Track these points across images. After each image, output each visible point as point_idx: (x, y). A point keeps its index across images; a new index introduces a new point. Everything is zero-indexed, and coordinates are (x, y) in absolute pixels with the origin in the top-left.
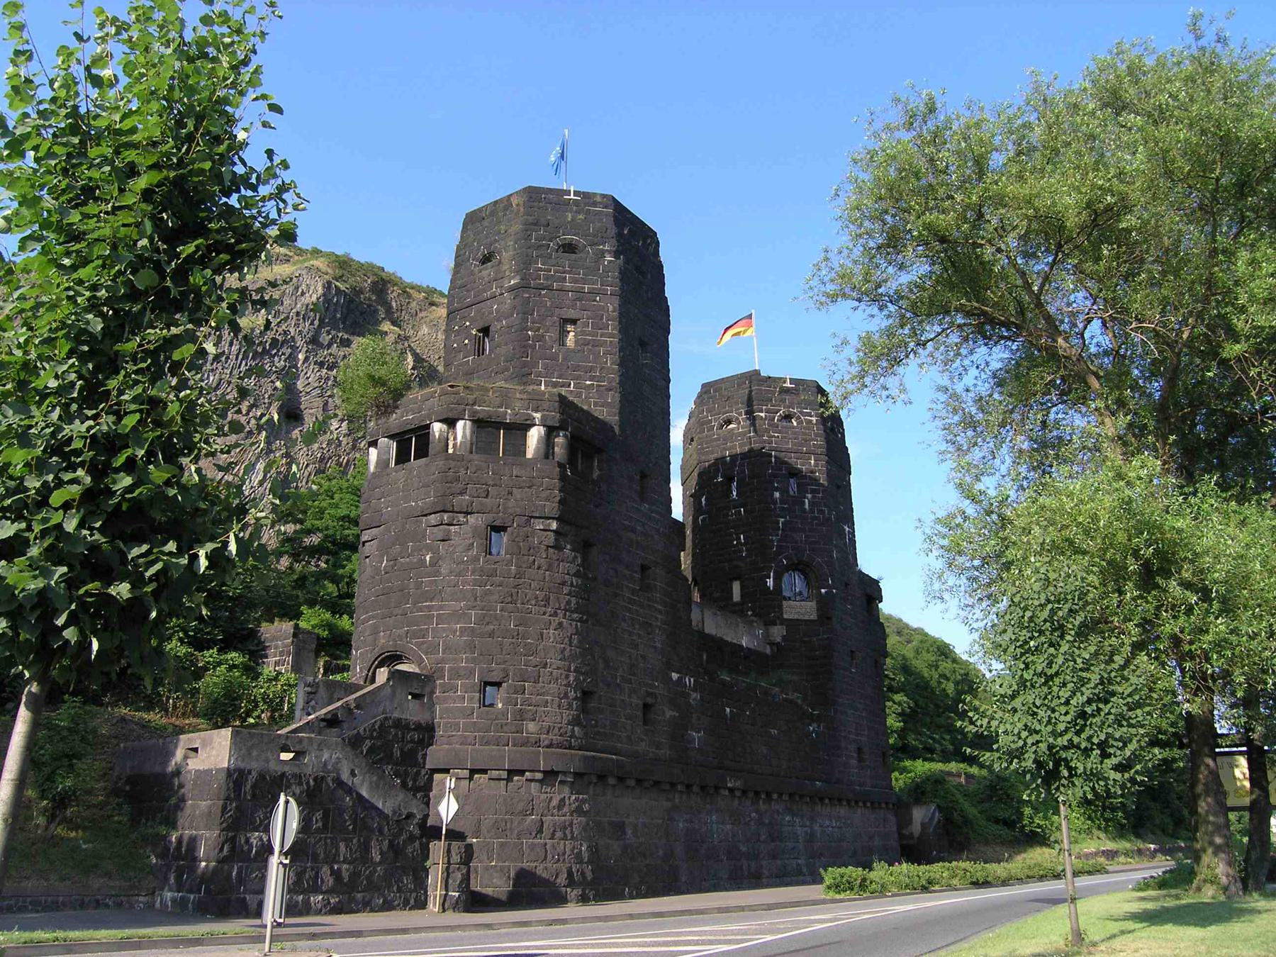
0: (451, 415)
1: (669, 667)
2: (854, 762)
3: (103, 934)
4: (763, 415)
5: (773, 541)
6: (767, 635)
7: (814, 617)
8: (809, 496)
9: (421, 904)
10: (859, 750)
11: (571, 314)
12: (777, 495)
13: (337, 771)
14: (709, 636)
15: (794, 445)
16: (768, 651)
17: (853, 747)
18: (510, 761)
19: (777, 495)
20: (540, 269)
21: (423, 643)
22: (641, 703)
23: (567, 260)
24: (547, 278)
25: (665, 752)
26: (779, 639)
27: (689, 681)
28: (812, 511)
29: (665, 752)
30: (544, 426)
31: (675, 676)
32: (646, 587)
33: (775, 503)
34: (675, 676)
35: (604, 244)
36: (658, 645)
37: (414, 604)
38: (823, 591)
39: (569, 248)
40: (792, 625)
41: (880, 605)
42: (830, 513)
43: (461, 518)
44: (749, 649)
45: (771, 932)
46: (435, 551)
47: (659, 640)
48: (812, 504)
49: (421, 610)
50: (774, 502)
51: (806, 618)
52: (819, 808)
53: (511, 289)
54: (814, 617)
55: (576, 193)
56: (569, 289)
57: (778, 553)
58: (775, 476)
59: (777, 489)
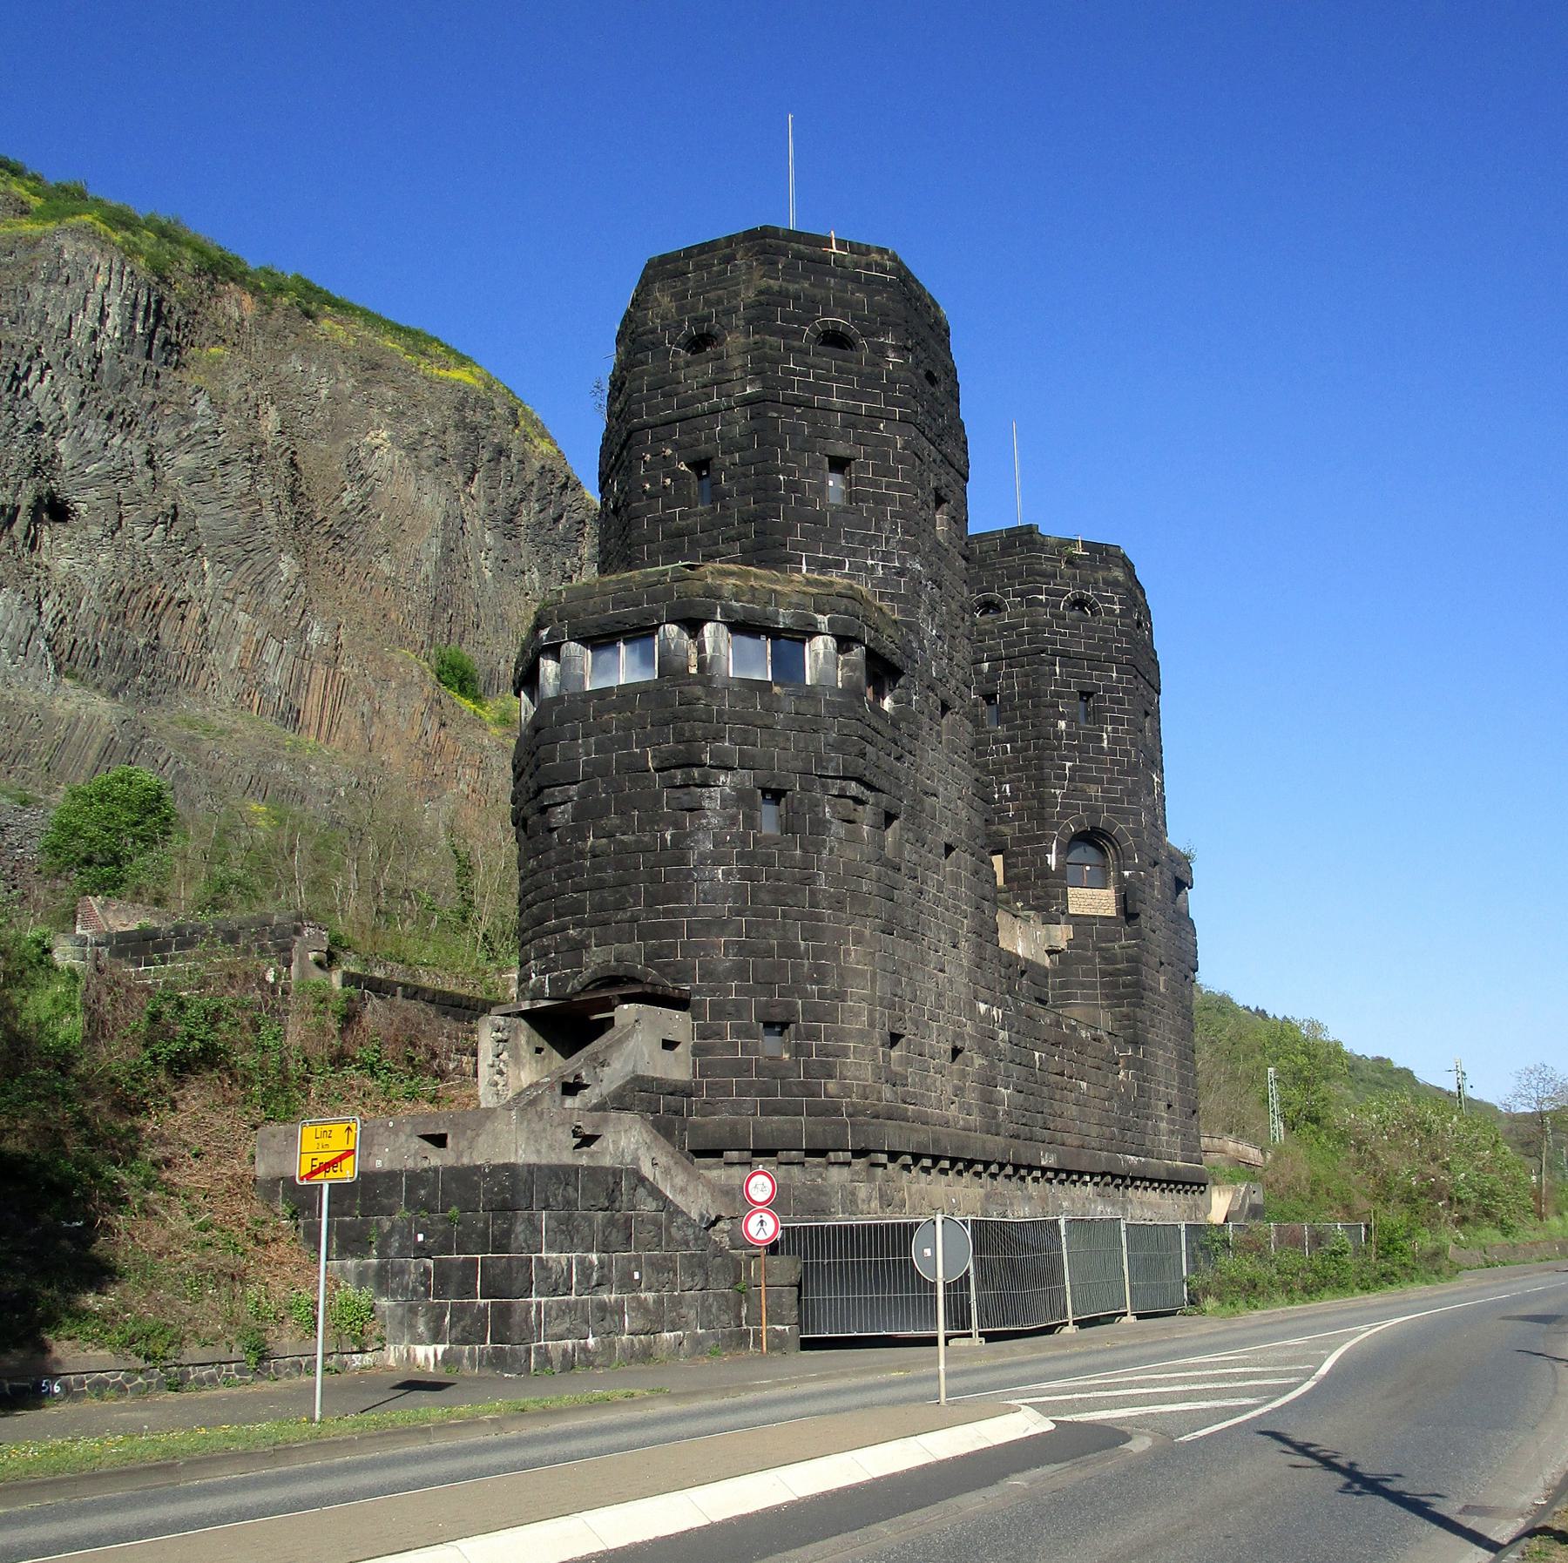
0: (692, 614)
7: (1111, 912)
11: (841, 449)
12: (1062, 724)
13: (636, 1159)
15: (1087, 646)
16: (1046, 961)
18: (810, 1137)
19: (1062, 724)
20: (794, 372)
21: (668, 965)
22: (949, 1047)
23: (830, 360)
24: (806, 386)
26: (1063, 945)
29: (975, 1119)
30: (833, 635)
31: (983, 1007)
35: (885, 335)
36: (965, 962)
37: (649, 905)
38: (1126, 873)
39: (835, 339)
40: (1079, 921)
42: (1137, 757)
43: (122, 654)
44: (1027, 960)
45: (1287, 1347)
46: (677, 825)
49: (667, 913)
51: (1101, 913)
53: (748, 402)
54: (1111, 912)
55: (842, 244)
56: (838, 407)
57: (1062, 816)
59: (1062, 716)
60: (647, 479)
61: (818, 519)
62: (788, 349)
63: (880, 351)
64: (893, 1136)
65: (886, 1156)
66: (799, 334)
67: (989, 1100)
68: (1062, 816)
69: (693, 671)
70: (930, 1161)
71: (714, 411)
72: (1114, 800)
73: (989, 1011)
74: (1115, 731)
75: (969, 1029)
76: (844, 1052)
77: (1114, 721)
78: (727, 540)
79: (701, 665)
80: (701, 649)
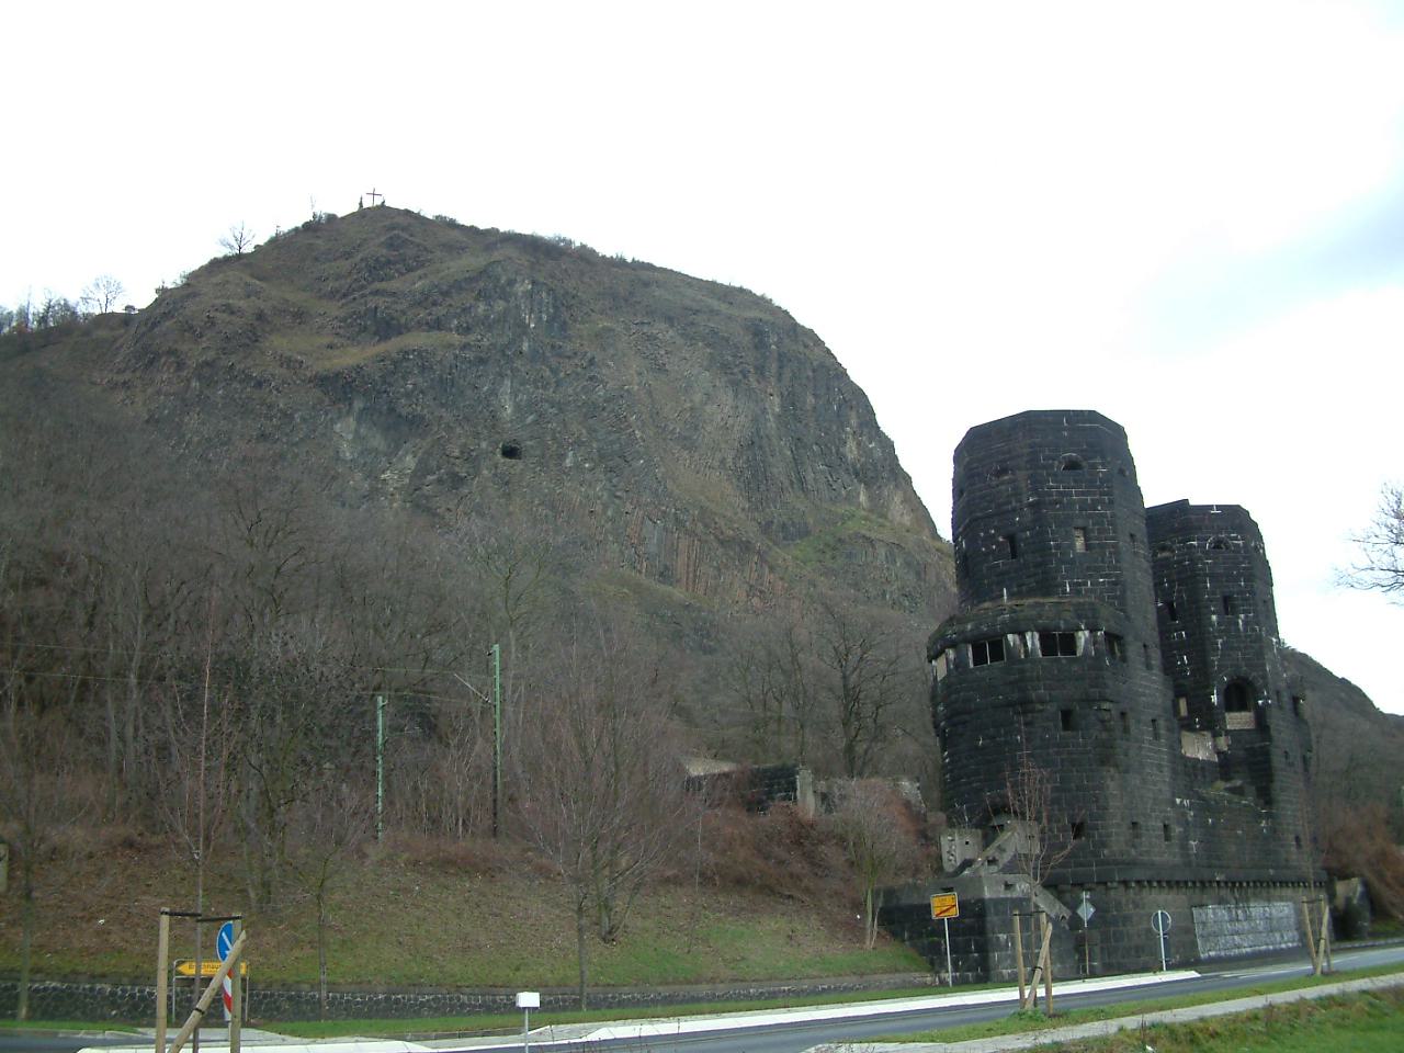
1: (1174, 795)
2: (1293, 849)
3: (108, 1035)
4: (1195, 543)
5: (1213, 661)
6: (1215, 746)
8: (1242, 616)
9: (14, 1016)
10: (1297, 839)
12: (1214, 617)
14: (1188, 758)
17: (1292, 837)
19: (1214, 617)
22: (1162, 825)
25: (1178, 860)
27: (1186, 802)
28: (1245, 630)
29: (1178, 860)
31: (1178, 801)
32: (1156, 736)
33: (1213, 626)
34: (1178, 801)
38: (1260, 702)
39: (1072, 466)
41: (144, 305)
47: (1167, 772)
48: (1246, 623)
50: (1212, 625)
52: (1272, 891)
53: (1031, 505)
54: (1252, 726)
57: (1220, 671)
58: (1210, 600)
59: (1214, 613)
60: (983, 546)
61: (1072, 562)
62: (1048, 475)
63: (1094, 466)
64: (1139, 874)
65: (1218, 739)
66: (1052, 466)
67: (1184, 847)
68: (1220, 671)
69: (1023, 657)
70: (1044, 995)
71: (1014, 510)
72: (1249, 659)
73: (1181, 802)
74: (1246, 617)
75: (1171, 814)
76: (1109, 835)
77: (1244, 612)
78: (1028, 577)
79: (1026, 651)
80: (1025, 645)
